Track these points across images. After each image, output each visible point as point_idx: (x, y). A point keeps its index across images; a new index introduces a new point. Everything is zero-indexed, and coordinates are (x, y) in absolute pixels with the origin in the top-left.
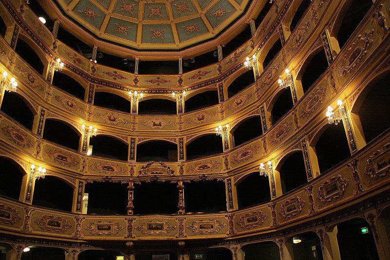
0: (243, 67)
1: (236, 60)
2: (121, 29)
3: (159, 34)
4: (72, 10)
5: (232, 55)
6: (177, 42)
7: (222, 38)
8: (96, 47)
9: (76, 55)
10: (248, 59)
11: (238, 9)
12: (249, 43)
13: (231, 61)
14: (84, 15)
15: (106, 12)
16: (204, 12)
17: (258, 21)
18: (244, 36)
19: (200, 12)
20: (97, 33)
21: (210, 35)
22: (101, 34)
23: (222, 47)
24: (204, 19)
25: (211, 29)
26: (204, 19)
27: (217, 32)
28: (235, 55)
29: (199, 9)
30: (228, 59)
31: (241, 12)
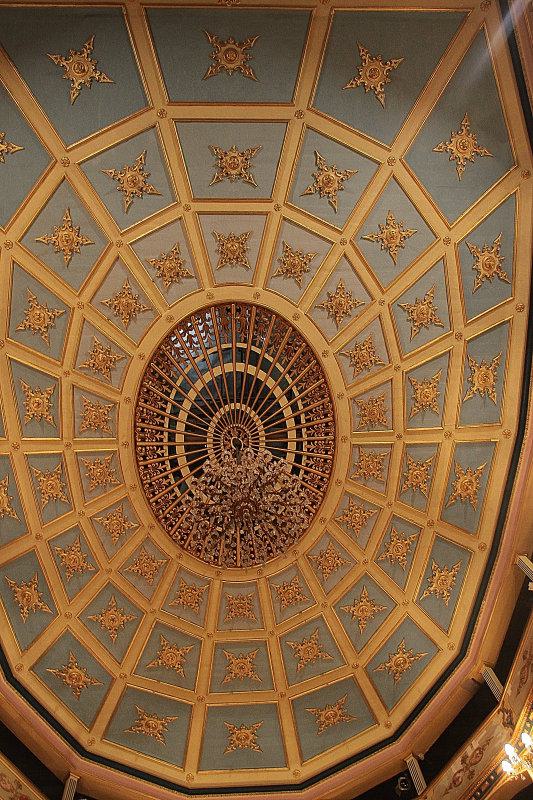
0: (500, 784)
1: (472, 773)
2: (148, 725)
3: (247, 738)
4: (32, 669)
5: (456, 766)
6: (295, 765)
7: (415, 735)
8: (74, 778)
9: (20, 786)
10: (509, 749)
11: (443, 645)
12: (496, 718)
13: (455, 782)
14: (57, 685)
15: (116, 672)
16: (363, 661)
17: (502, 668)
18: (478, 705)
19: (352, 661)
20: (84, 738)
21: (380, 733)
22: (92, 742)
23: (420, 761)
24: (364, 683)
25: (381, 715)
26: (364, 683)
27: (397, 719)
28: (463, 761)
29: (349, 654)
30: (444, 779)
31: (454, 653)
